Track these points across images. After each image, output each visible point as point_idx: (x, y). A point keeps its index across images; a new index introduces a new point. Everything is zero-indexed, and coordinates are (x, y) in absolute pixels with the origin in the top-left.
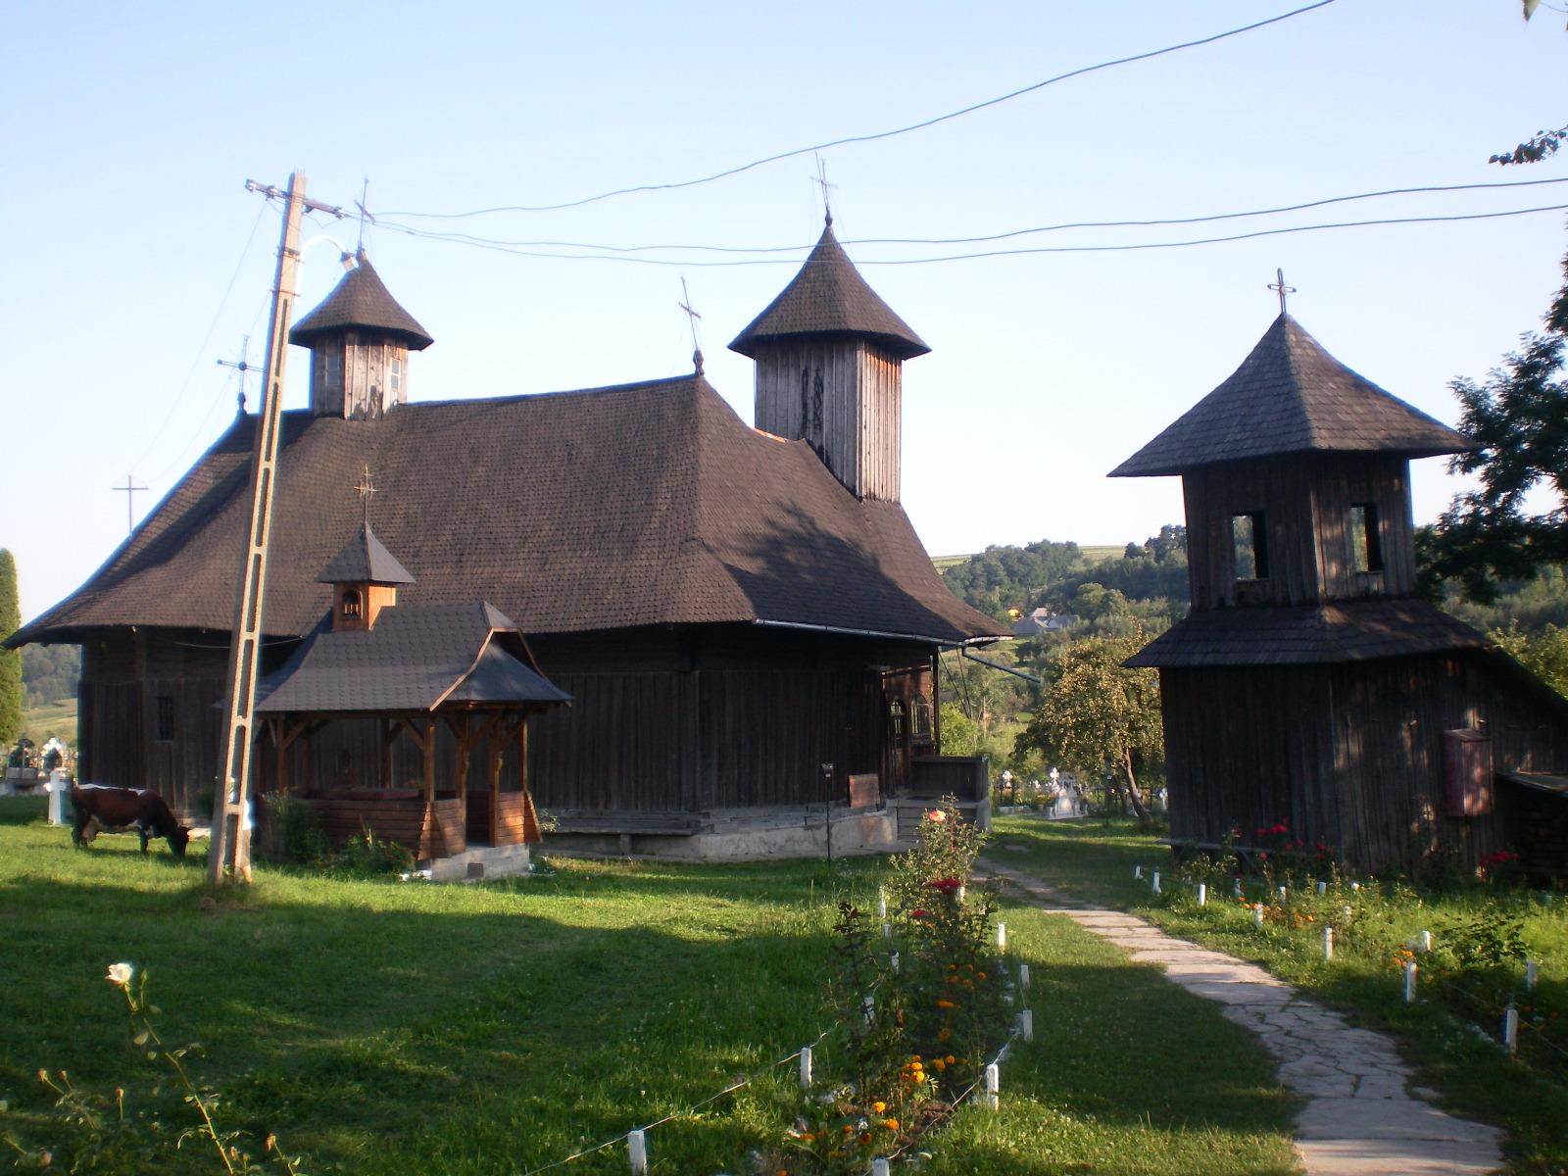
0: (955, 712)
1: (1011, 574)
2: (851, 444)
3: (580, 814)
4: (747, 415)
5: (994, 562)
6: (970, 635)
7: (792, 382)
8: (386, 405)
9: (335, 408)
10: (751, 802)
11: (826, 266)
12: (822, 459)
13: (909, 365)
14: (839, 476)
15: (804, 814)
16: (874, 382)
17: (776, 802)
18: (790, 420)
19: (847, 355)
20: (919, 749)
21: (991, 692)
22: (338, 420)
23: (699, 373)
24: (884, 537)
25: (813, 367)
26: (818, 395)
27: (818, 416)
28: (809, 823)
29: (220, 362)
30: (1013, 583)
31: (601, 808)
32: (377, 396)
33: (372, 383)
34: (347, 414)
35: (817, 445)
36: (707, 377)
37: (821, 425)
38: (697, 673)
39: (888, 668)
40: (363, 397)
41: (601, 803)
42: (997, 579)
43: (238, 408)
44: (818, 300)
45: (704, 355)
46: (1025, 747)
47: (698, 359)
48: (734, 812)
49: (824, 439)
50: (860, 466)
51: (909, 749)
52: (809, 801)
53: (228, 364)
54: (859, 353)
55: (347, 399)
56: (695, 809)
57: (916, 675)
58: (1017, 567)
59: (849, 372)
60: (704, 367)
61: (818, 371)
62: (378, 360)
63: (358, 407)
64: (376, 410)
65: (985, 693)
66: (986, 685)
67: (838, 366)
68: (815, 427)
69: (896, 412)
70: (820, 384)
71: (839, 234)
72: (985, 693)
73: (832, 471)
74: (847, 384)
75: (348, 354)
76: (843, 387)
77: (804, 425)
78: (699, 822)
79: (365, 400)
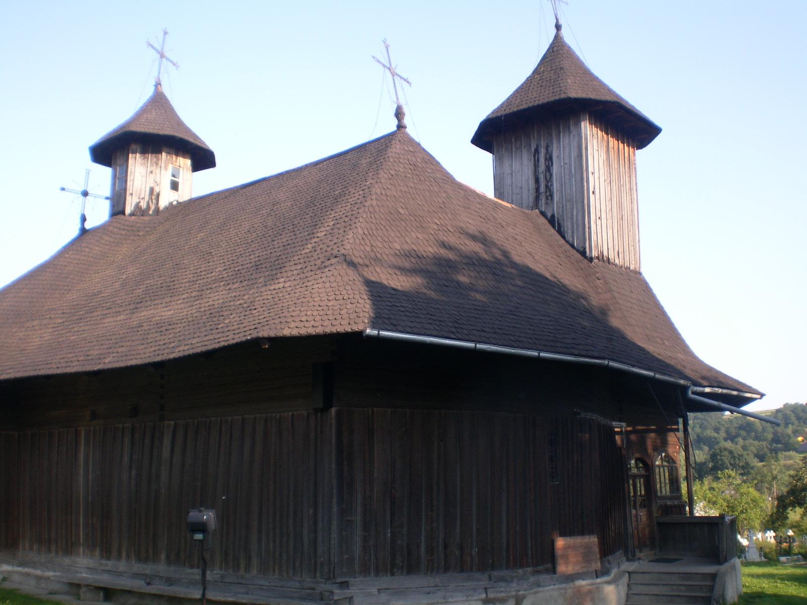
0: (751, 490)
1: (799, 418)
2: (580, 208)
3: (222, 577)
4: (490, 193)
5: (788, 413)
6: (705, 383)
7: (525, 161)
8: (163, 203)
9: (121, 209)
10: (411, 567)
11: (557, 56)
12: (554, 227)
13: (642, 156)
14: (570, 240)
15: (485, 583)
16: (603, 155)
17: (446, 569)
18: (525, 196)
19: (572, 128)
20: (666, 510)
21: (779, 477)
22: (121, 216)
23: (401, 127)
24: (616, 295)
25: (543, 143)
26: (548, 169)
27: (548, 188)
28: (491, 595)
29: (63, 189)
30: (800, 423)
31: (242, 572)
32: (154, 195)
33: (151, 184)
34: (128, 211)
35: (549, 215)
36: (412, 131)
37: (552, 196)
38: (333, 410)
39: (624, 424)
40: (142, 196)
41: (242, 565)
42: (791, 421)
43: (79, 226)
44: (544, 84)
45: (406, 109)
46: (785, 507)
47: (399, 114)
48: (385, 581)
49: (555, 208)
50: (590, 228)
51: (654, 510)
52: (493, 568)
53: (70, 191)
54: (583, 124)
55: (128, 198)
56: (330, 577)
57: (663, 432)
58: (801, 414)
59: (574, 144)
60: (406, 121)
61: (547, 148)
62: (157, 164)
63: (137, 206)
64: (153, 207)
65: (774, 478)
66: (775, 472)
67: (565, 140)
68: (547, 198)
69: (632, 190)
70: (549, 159)
71: (568, 37)
72: (774, 478)
73: (564, 237)
74: (574, 154)
75: (131, 161)
76: (570, 157)
77: (537, 198)
78: (332, 593)
79: (143, 198)
